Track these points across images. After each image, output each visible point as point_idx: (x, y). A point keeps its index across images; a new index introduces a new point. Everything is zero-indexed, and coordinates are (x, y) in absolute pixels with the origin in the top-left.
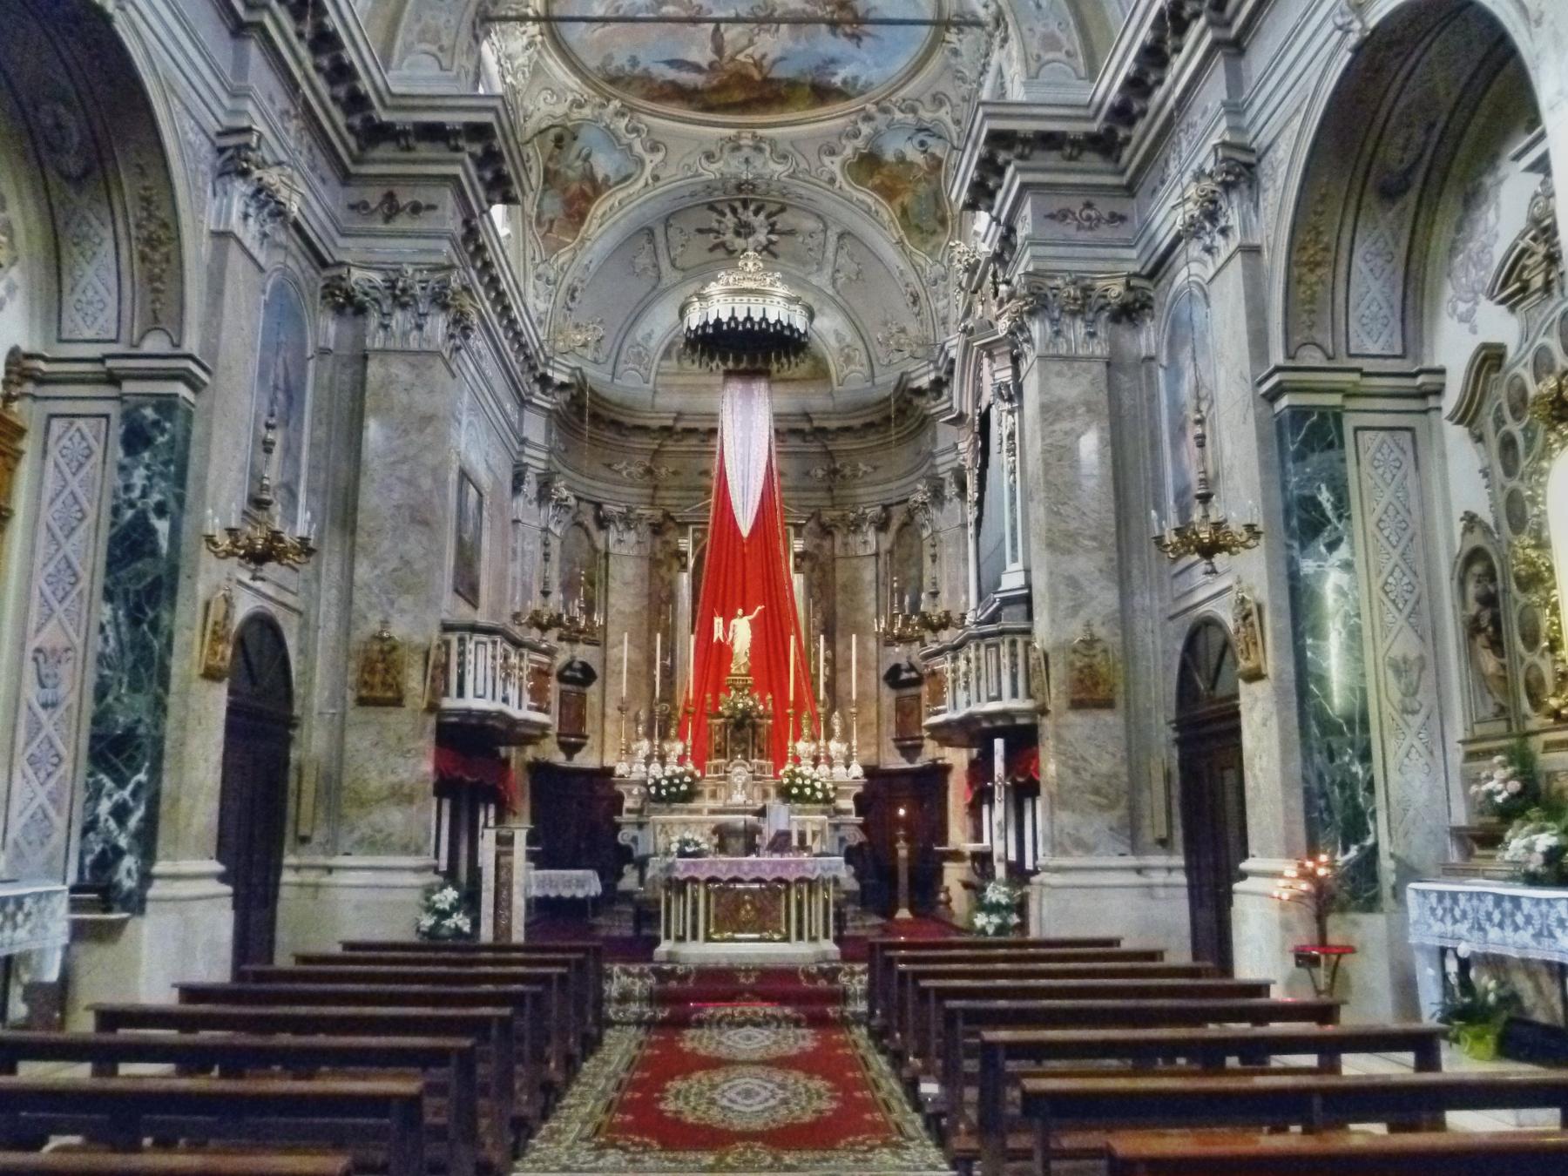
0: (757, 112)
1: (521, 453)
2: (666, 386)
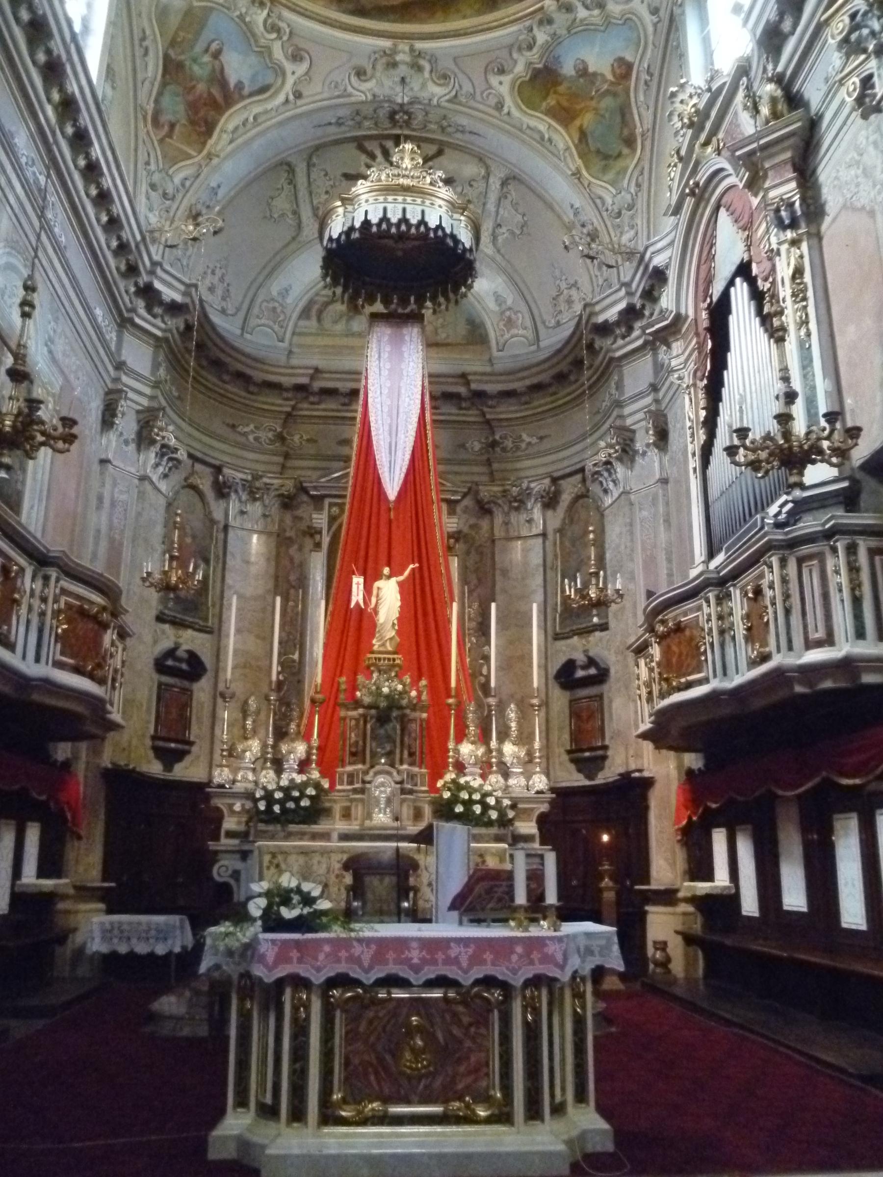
1: (117, 380)
2: (300, 346)
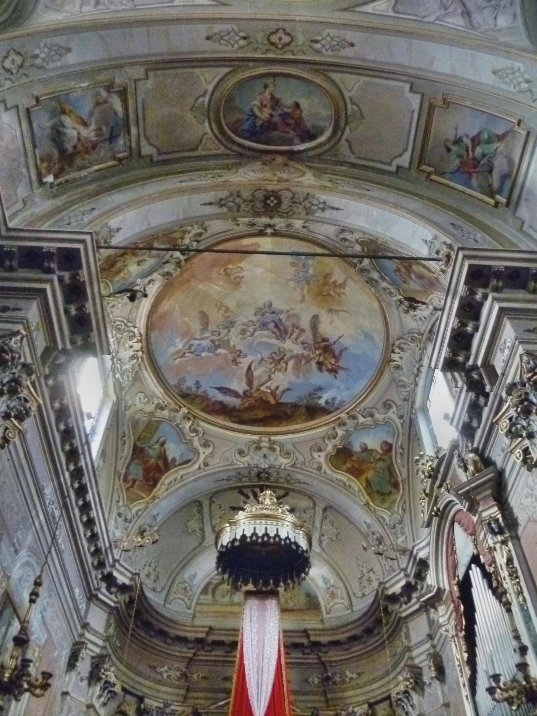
0: (272, 425)
1: (81, 635)
2: (200, 612)
